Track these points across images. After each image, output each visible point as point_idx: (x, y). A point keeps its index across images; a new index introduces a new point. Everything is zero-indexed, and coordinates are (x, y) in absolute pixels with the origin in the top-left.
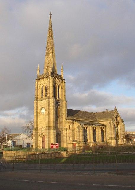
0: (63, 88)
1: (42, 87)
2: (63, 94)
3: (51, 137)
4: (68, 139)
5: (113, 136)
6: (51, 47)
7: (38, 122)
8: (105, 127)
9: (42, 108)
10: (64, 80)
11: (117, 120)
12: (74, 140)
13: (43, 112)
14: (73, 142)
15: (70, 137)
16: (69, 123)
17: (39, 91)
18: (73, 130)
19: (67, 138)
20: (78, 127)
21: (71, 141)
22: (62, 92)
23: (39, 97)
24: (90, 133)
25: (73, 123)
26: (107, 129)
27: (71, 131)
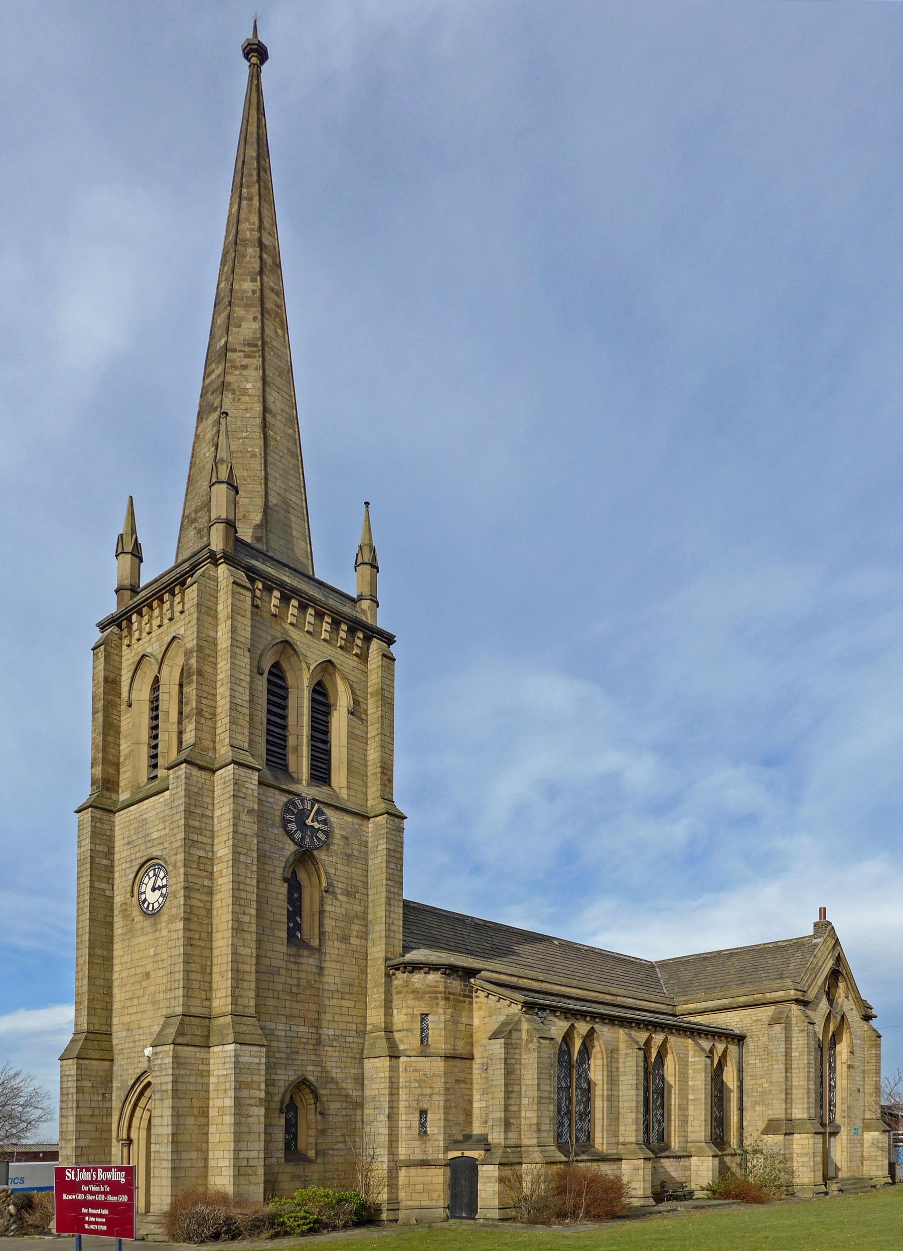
0: (373, 708)
1: (156, 685)
2: (373, 755)
3: (212, 1113)
4: (403, 1132)
5: (799, 1112)
6: (249, 328)
7: (116, 991)
8: (733, 1049)
9: (148, 864)
10: (389, 640)
11: (831, 1001)
12: (468, 1137)
13: (153, 897)
14: (447, 1149)
15: (423, 1113)
16: (417, 994)
17: (125, 724)
18: (459, 1057)
19: (392, 1117)
20: (506, 1032)
21: (436, 1148)
22: (356, 738)
23: (125, 778)
24: (613, 1079)
25: (460, 1002)
26: (751, 1060)
27: (439, 1065)
